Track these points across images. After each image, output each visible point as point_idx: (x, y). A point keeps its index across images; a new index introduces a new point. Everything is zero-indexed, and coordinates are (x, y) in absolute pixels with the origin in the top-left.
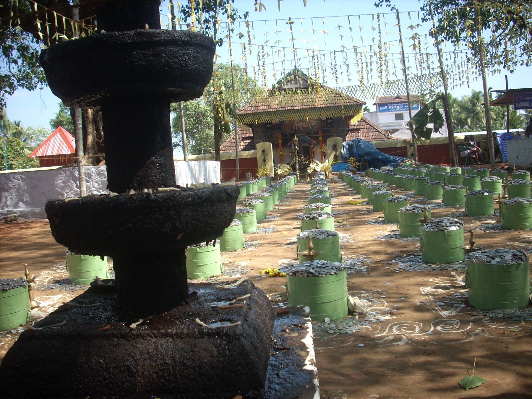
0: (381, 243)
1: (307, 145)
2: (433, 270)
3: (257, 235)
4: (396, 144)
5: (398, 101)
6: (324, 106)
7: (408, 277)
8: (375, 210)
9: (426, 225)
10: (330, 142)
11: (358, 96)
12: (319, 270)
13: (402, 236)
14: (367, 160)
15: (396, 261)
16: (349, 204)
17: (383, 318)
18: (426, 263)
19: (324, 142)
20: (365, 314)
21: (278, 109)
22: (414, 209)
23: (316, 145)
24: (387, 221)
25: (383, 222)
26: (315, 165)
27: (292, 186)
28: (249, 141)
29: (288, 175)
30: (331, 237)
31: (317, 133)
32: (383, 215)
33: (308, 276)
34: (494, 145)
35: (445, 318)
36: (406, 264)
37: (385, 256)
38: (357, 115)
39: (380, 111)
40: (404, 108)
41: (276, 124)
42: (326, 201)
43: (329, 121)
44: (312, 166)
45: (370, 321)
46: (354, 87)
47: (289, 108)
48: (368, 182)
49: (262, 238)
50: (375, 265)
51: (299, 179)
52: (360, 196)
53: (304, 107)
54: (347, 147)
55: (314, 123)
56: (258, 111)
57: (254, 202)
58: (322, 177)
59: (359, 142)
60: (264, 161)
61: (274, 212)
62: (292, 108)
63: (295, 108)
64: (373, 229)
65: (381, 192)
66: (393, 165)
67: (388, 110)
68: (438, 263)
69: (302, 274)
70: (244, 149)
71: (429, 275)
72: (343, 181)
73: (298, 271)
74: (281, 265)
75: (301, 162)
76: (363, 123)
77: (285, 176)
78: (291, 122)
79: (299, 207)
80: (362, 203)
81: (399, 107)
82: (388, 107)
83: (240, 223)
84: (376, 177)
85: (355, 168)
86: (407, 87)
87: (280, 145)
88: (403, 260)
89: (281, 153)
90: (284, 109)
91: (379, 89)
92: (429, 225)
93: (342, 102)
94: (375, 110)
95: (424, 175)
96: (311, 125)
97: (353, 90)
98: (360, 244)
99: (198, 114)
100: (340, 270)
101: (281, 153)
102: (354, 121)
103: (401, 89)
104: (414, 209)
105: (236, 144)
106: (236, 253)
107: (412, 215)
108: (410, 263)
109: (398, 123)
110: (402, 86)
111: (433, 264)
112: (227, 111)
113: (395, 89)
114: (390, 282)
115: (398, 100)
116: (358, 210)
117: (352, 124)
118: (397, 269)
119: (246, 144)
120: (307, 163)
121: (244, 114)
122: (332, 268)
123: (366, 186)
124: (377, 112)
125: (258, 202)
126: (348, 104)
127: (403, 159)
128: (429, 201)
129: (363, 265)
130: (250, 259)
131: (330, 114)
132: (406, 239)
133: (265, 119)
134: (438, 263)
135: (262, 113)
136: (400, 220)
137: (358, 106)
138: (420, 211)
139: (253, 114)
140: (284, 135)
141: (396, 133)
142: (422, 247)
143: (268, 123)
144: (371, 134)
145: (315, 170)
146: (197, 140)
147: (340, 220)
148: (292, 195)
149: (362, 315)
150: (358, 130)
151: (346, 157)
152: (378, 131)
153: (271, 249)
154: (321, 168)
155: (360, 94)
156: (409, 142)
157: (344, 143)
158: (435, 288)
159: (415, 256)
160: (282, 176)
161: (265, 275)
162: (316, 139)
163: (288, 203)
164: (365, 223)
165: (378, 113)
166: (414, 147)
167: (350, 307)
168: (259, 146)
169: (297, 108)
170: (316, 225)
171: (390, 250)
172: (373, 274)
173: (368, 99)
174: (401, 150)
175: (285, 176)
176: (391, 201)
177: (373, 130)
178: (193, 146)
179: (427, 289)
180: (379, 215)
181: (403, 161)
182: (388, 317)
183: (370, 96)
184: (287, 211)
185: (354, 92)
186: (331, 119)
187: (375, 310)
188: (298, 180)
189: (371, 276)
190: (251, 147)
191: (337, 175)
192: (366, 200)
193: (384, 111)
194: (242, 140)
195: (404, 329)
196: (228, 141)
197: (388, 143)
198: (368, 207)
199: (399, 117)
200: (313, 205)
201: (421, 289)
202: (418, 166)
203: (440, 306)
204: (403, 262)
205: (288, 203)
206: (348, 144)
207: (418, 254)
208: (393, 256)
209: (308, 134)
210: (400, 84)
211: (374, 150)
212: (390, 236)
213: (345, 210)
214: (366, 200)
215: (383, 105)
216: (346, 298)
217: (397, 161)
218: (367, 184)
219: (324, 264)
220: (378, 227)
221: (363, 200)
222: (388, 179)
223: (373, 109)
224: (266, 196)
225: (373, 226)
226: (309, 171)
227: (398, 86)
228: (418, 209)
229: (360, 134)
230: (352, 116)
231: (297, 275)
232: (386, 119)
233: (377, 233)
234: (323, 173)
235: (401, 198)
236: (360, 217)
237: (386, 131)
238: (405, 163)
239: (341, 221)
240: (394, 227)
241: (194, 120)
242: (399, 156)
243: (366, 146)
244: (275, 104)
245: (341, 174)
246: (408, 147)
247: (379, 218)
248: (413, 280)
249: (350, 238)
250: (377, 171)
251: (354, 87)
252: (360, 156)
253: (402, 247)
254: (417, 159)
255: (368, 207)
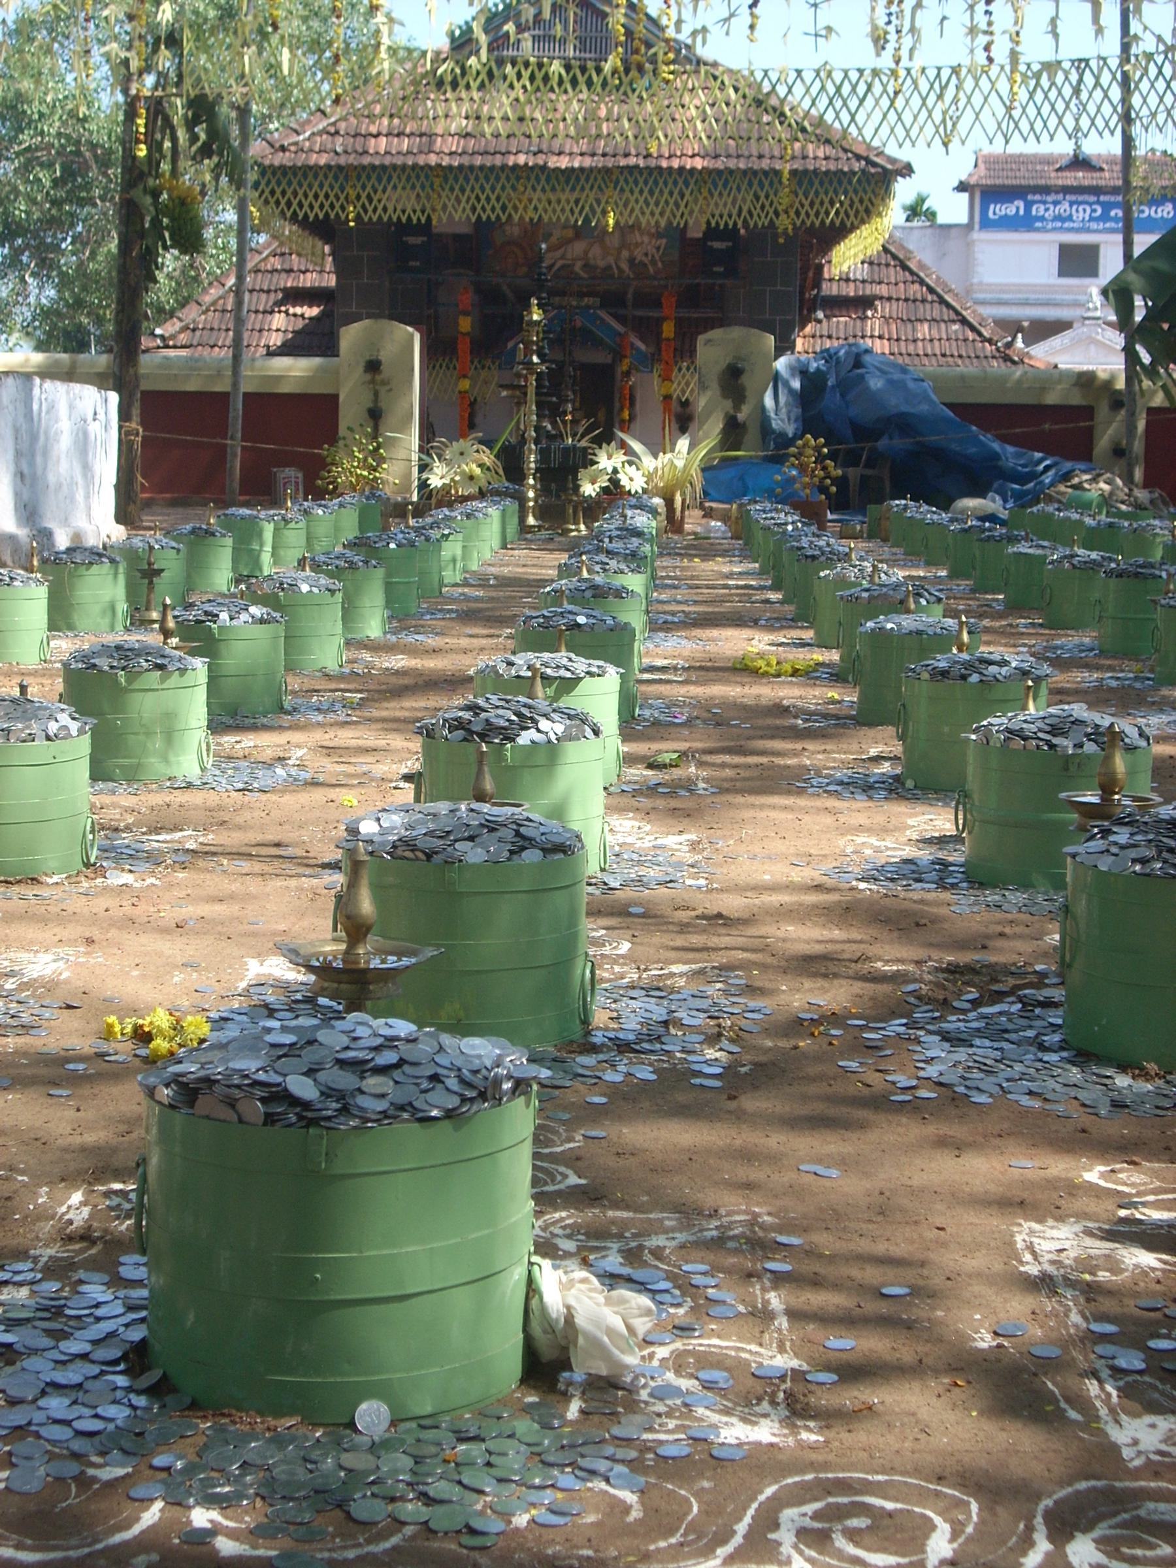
0: (848, 911)
1: (601, 357)
2: (1117, 1105)
3: (195, 798)
4: (1043, 390)
5: (1077, 178)
6: (699, 163)
7: (958, 1147)
8: (866, 717)
9: (1105, 833)
10: (713, 348)
11: (873, 128)
12: (345, 1080)
13: (978, 877)
14: (886, 454)
15: (912, 1025)
16: (743, 669)
17: (734, 1432)
18: (1083, 1056)
19: (685, 349)
20: (631, 1390)
21: (466, 160)
22: (1055, 730)
23: (648, 361)
24: (910, 785)
25: (896, 789)
26: (619, 458)
27: (488, 555)
28: (315, 311)
29: (482, 495)
30: (532, 856)
31: (658, 304)
32: (897, 749)
33: (270, 1119)
34: (1142, 1490)
35: (1136, 1474)
36: (962, 1054)
37: (858, 987)
38: (865, 230)
39: (986, 224)
40: (1105, 217)
41: (457, 237)
42: (610, 644)
43: (717, 245)
44: (607, 461)
45: (645, 1448)
46: (854, 75)
47: (522, 159)
48: (863, 564)
49: (216, 819)
50: (784, 1044)
51: (531, 521)
52: (808, 635)
53: (598, 162)
54: (796, 384)
55: (647, 248)
56: (366, 160)
57: (224, 616)
58: (641, 520)
59: (858, 363)
60: (375, 415)
61: (341, 677)
62: (540, 160)
63: (554, 162)
64: (828, 820)
65: (908, 622)
66: (1018, 496)
67: (1025, 223)
68: (1152, 1067)
69: (232, 1104)
70: (289, 349)
71: (1085, 1141)
72: (746, 554)
73: (209, 1081)
74: (246, 993)
75: (551, 437)
76: (893, 274)
77: (464, 499)
78: (534, 230)
79: (472, 665)
80: (808, 674)
81: (1081, 214)
82: (1028, 206)
83: (74, 726)
84: (917, 545)
85: (823, 489)
86: (1126, 100)
87: (464, 346)
88: (953, 1023)
89: (465, 384)
90: (498, 160)
91: (977, 100)
92: (1122, 836)
93: (782, 153)
94: (964, 219)
95: (1158, 554)
96: (631, 261)
97: (846, 89)
98: (732, 904)
99: (78, 153)
100: (483, 1096)
101: (465, 384)
102: (848, 258)
103: (1092, 108)
104: (1055, 730)
105: (239, 321)
106: (29, 891)
107: (1045, 764)
108: (984, 1050)
109: (1068, 290)
110: (1098, 95)
111: (1123, 1068)
112: (194, 138)
113: (1060, 106)
114: (843, 1163)
115: (1081, 177)
116: (780, 710)
117: (836, 272)
118: (903, 1080)
119: (300, 324)
120: (584, 443)
121: (294, 169)
122: (435, 1078)
123: (842, 582)
124: (969, 227)
125: (244, 617)
126: (824, 166)
127: (1068, 465)
128: (1165, 692)
129: (713, 1039)
130: (90, 941)
131: (722, 209)
132: (993, 897)
133: (399, 203)
134: (1152, 1067)
135: (383, 173)
136: (973, 783)
137: (872, 180)
138: (1090, 747)
139: (339, 173)
140: (489, 296)
141: (1056, 342)
142: (1065, 957)
143: (404, 228)
144: (923, 330)
145: (615, 481)
146: (64, 282)
147: (667, 750)
148: (468, 599)
149: (610, 1391)
150: (863, 303)
151: (782, 435)
152: (964, 321)
153: (235, 887)
154: (649, 477)
155: (877, 116)
156: (1108, 384)
157: (781, 364)
158: (1110, 1235)
159: (1028, 1005)
160: (446, 498)
161: (122, 1050)
162: (649, 329)
163: (431, 641)
164: (793, 782)
165: (976, 235)
166: (1132, 414)
167: (536, 1329)
168: (351, 336)
169: (563, 163)
170: (480, 773)
171: (892, 957)
172: (751, 1103)
173: (921, 143)
174: (1063, 424)
175: (464, 499)
176: (944, 674)
177: (937, 311)
178: (46, 314)
179: (1054, 1242)
180: (880, 746)
181: (1066, 477)
182: (765, 1432)
183: (929, 129)
184: (406, 681)
185: (853, 103)
186: (730, 234)
187: (705, 1360)
188: (524, 528)
189: (740, 1117)
190: (313, 340)
191: (725, 518)
192: (834, 656)
193: (1008, 224)
194: (279, 303)
195: (853, 1535)
196: (207, 299)
197: (1002, 381)
198: (833, 694)
199: (1077, 261)
200: (520, 659)
201: (1024, 1232)
202: (1138, 506)
203: (1117, 1372)
204: (946, 1037)
205: (431, 641)
206: (802, 371)
207: (1042, 994)
208: (901, 1004)
209: (613, 301)
210: (1089, 79)
211: (931, 404)
212: (910, 871)
213: (705, 705)
214: (834, 656)
215: (1003, 193)
216: (518, 1274)
217: (1033, 476)
218: (851, 574)
219: (390, 1042)
220: (858, 810)
221: (819, 656)
222: (976, 565)
223: (953, 209)
224: (305, 588)
225: (832, 803)
226: (589, 489)
227: (1077, 91)
228: (1077, 735)
229: (874, 325)
230: (839, 232)
231: (204, 1104)
232: (1013, 267)
233: (845, 844)
234: (657, 501)
235: (1004, 663)
236: (778, 745)
237: (1013, 327)
238: (1078, 487)
239: (666, 758)
240: (940, 820)
241: (56, 183)
242: (1049, 453)
243: (891, 382)
244: (453, 126)
245: (744, 514)
246: (1103, 411)
247: (877, 759)
248: (983, 1169)
249: (690, 858)
250: (928, 513)
251: (854, 75)
252: (864, 432)
253: (961, 945)
254: (1138, 474)
255: (833, 694)
